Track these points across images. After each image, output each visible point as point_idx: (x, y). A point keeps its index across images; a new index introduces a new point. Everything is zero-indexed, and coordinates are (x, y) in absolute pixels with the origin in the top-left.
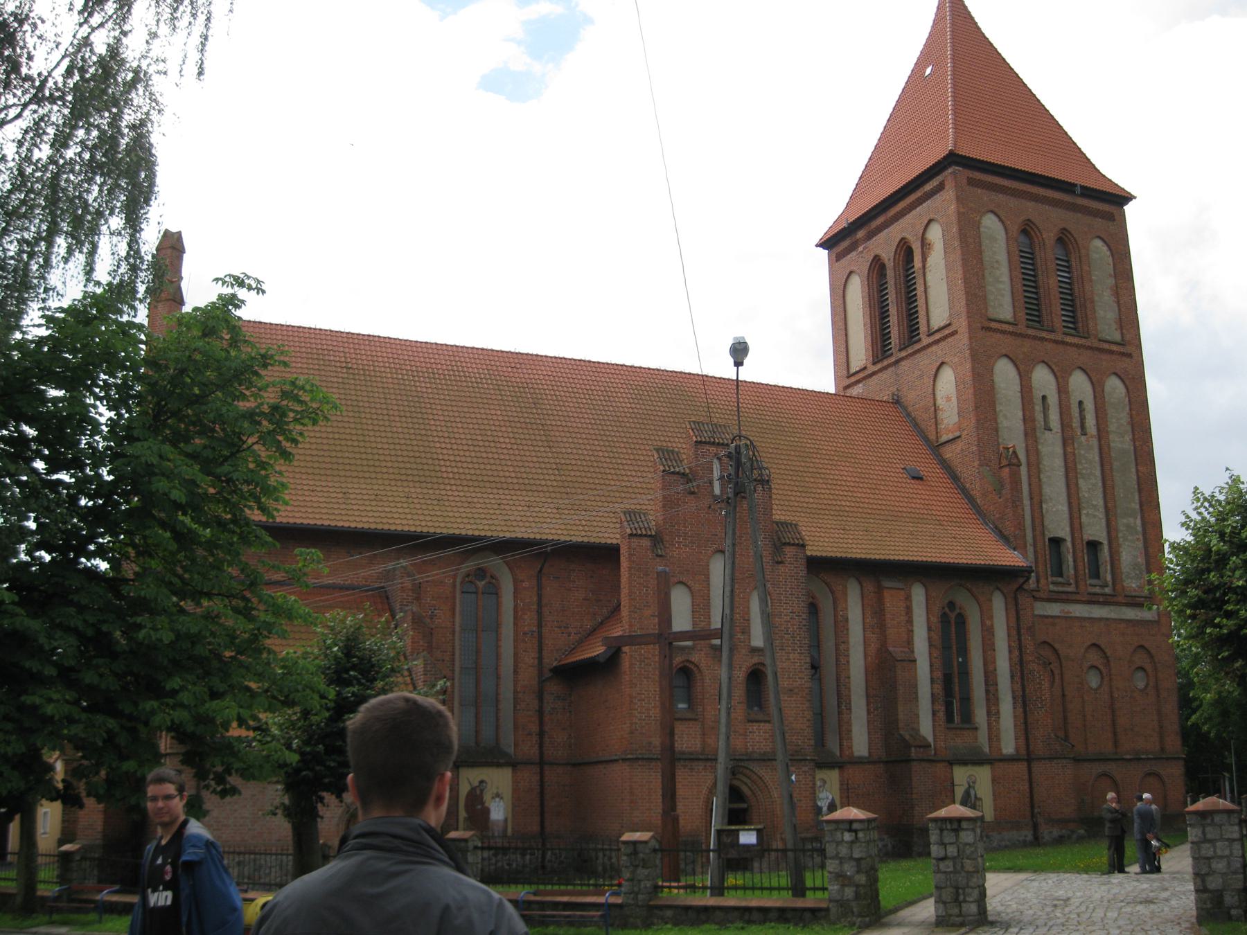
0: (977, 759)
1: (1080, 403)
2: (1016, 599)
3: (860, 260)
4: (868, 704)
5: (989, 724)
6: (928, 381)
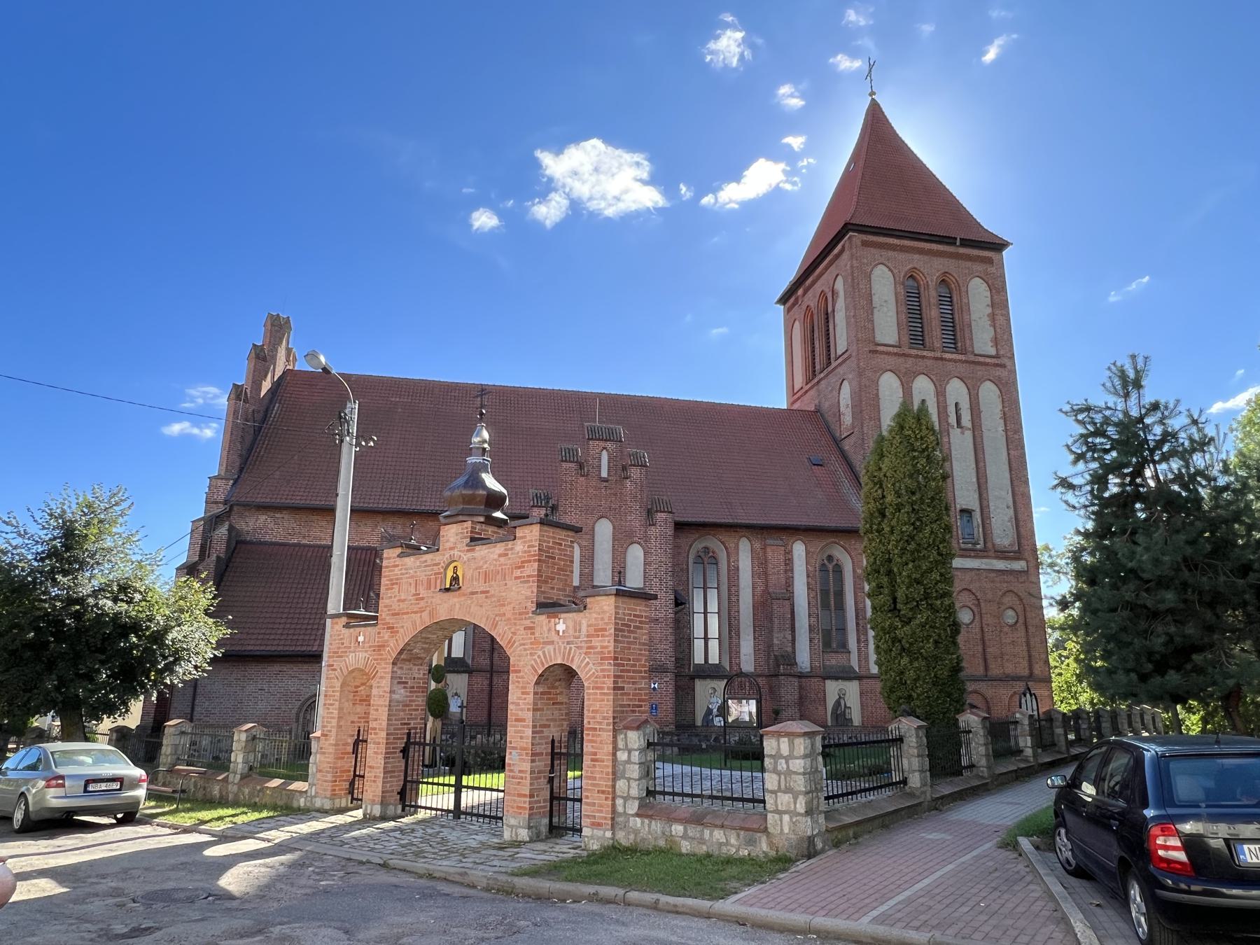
0: (846, 674)
1: (957, 404)
3: (798, 312)
5: (859, 650)
6: (835, 393)
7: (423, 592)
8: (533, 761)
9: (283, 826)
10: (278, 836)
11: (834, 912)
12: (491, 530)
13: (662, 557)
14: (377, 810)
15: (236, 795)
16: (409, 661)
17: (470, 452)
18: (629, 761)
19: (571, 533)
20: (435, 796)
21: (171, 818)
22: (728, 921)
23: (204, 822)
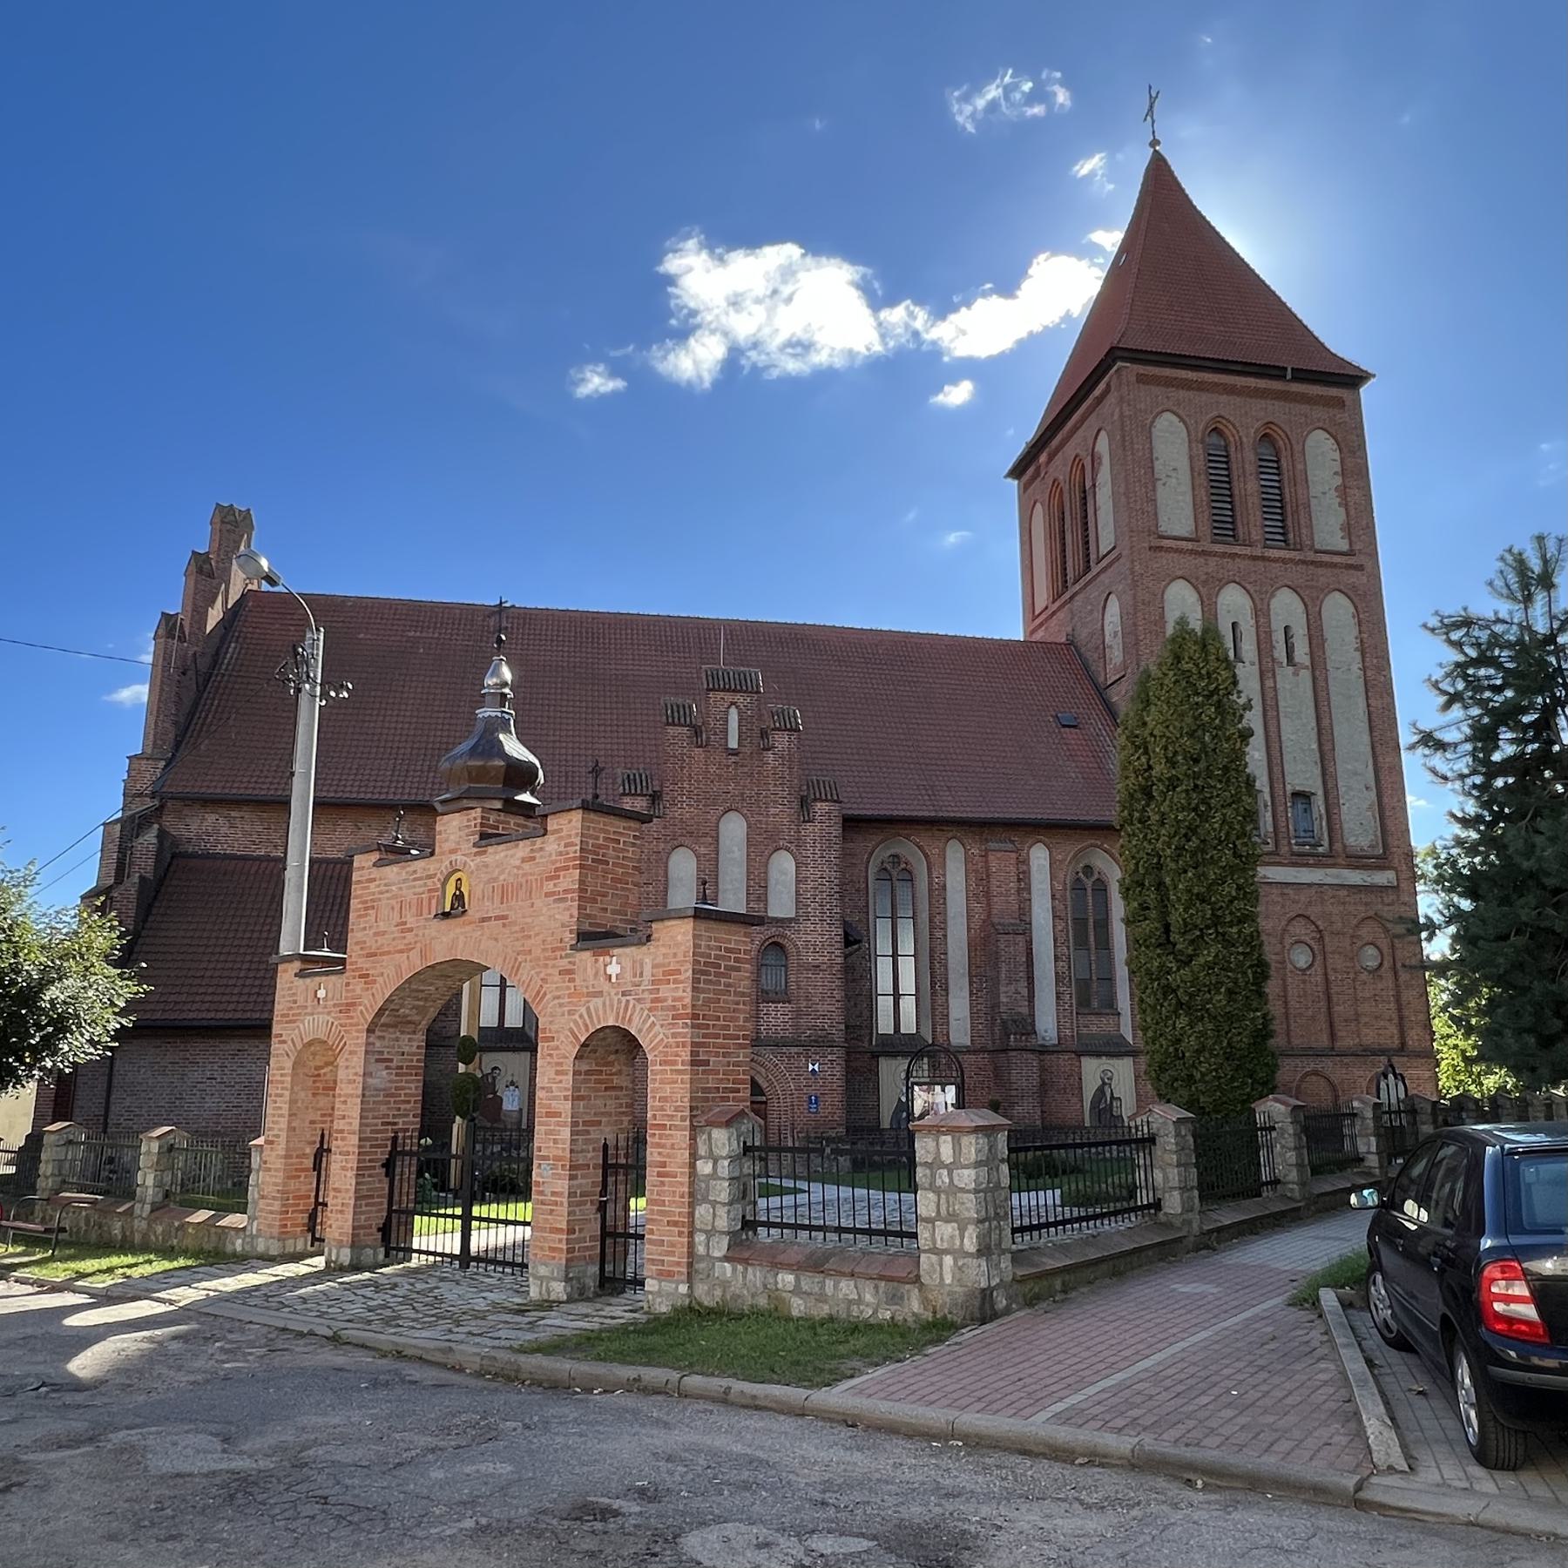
0: (1114, 1048)
1: (1286, 628)
3: (1041, 489)
4: (971, 984)
7: (411, 921)
8: (572, 1178)
9: (199, 1281)
10: (186, 1295)
11: (995, 1406)
12: (513, 821)
13: (824, 871)
14: (345, 1256)
15: (145, 1236)
16: (395, 1026)
17: (481, 701)
18: (714, 1175)
19: (633, 824)
20: (435, 1235)
21: (36, 1270)
22: (831, 1420)
23: (82, 1276)
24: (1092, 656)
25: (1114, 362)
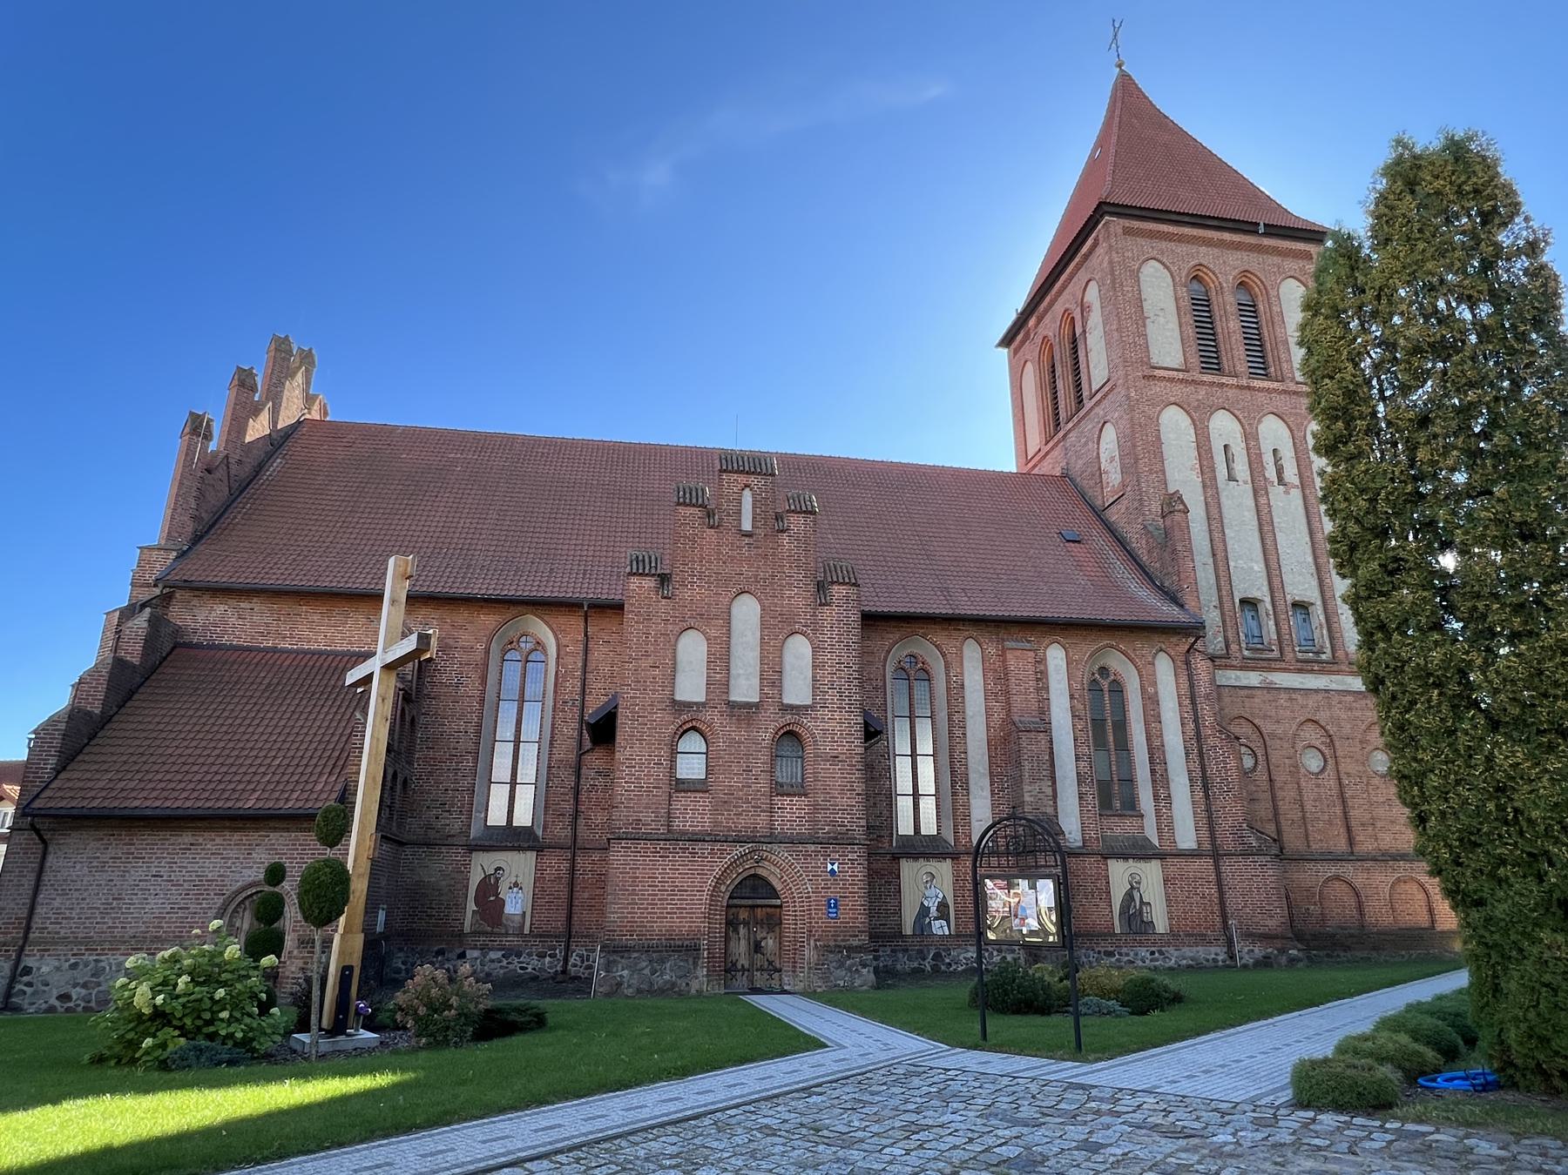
0: (1139, 851)
1: (1275, 451)
2: (1188, 663)
3: (1031, 350)
5: (1157, 811)
24: (1085, 483)
25: (1102, 216)
